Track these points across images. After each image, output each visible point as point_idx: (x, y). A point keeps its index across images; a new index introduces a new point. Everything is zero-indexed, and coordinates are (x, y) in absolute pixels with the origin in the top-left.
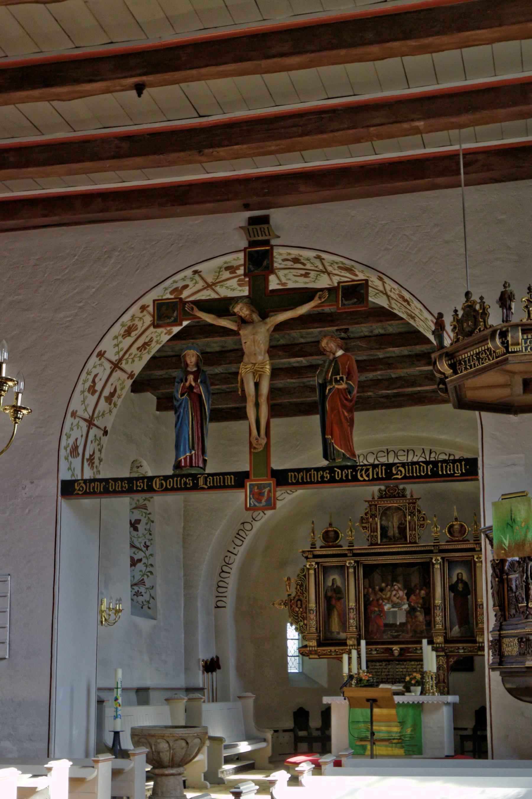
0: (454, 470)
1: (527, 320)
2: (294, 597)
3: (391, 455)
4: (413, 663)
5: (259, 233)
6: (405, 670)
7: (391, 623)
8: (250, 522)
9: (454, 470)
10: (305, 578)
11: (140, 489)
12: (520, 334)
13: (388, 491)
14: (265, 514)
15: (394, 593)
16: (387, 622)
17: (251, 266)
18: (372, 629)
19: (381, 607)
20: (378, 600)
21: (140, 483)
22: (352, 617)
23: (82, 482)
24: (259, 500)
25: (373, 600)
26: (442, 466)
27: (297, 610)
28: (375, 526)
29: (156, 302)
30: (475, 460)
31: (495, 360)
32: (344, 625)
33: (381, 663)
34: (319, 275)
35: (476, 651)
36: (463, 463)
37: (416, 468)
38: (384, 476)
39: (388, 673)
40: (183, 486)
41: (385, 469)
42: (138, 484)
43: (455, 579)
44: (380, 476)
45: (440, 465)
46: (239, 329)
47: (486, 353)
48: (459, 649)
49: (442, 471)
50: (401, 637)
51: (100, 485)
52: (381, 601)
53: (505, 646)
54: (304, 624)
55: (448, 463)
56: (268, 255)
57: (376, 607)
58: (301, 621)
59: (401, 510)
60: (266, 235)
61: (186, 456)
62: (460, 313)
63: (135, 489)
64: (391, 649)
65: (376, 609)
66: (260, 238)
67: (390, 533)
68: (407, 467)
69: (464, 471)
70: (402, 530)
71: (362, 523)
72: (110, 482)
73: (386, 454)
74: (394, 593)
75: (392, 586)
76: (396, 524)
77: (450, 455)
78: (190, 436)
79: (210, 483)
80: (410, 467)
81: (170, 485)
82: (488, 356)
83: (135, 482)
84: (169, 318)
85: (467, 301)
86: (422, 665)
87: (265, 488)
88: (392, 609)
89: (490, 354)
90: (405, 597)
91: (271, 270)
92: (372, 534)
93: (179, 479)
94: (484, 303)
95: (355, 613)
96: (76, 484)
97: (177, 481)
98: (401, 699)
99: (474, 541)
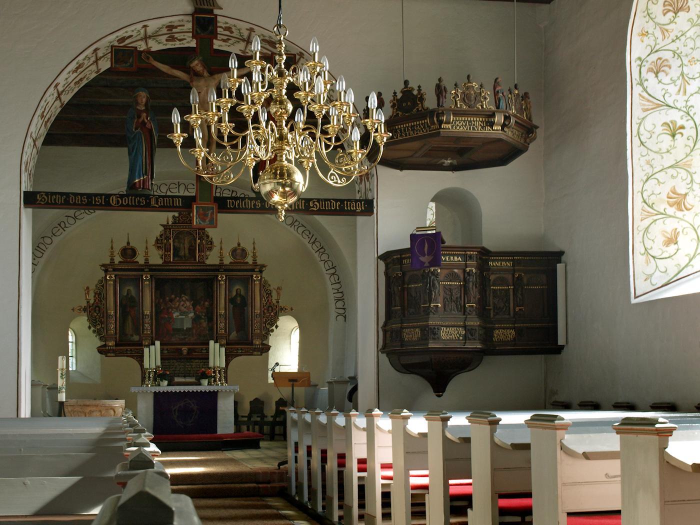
0: (356, 208)
1: (455, 107)
2: (93, 304)
3: (182, 187)
4: (197, 361)
5: (206, 4)
6: (190, 366)
7: (179, 328)
8: (50, 237)
9: (356, 208)
10: (104, 288)
11: (98, 204)
12: (452, 117)
13: (181, 218)
14: (64, 231)
15: (182, 303)
16: (174, 327)
17: (198, 30)
18: (162, 332)
19: (171, 314)
20: (168, 309)
21: (98, 198)
22: (147, 322)
23: (44, 194)
24: (204, 220)
25: (164, 309)
26: (347, 204)
27: (96, 314)
28: (169, 247)
29: (114, 48)
30: (372, 201)
31: (428, 132)
32: (137, 329)
33: (169, 361)
34: (238, 42)
35: (251, 351)
36: (363, 202)
37: (328, 203)
38: (303, 208)
39: (175, 369)
40: (137, 204)
41: (304, 202)
42: (97, 199)
43: (234, 293)
44: (300, 208)
45: (345, 202)
46: (192, 81)
47: (420, 127)
48: (238, 349)
49: (347, 208)
50: (187, 340)
51: (61, 198)
52: (171, 310)
53: (405, 334)
54: (101, 327)
55: (352, 202)
56: (213, 21)
57: (166, 314)
58: (99, 324)
59: (191, 234)
60: (211, 6)
61: (140, 180)
62: (399, 95)
63: (94, 203)
64: (181, 349)
65: (166, 316)
66: (206, 7)
67: (182, 253)
68: (50, 196)
69: (363, 208)
70: (192, 251)
71: (158, 243)
72: (70, 196)
73: (177, 186)
74: (182, 303)
75: (181, 297)
76: (187, 246)
77: (233, 191)
78: (144, 163)
79: (161, 203)
80: (323, 202)
81: (125, 202)
82: (422, 129)
83: (93, 198)
84: (126, 63)
85: (405, 88)
86: (208, 362)
87: (208, 210)
88: (180, 317)
89: (424, 127)
90: (191, 306)
91: (215, 35)
92: (166, 253)
93: (133, 198)
94: (421, 90)
95: (149, 319)
96: (38, 196)
97: (131, 199)
98: (182, 389)
99: (253, 263)
